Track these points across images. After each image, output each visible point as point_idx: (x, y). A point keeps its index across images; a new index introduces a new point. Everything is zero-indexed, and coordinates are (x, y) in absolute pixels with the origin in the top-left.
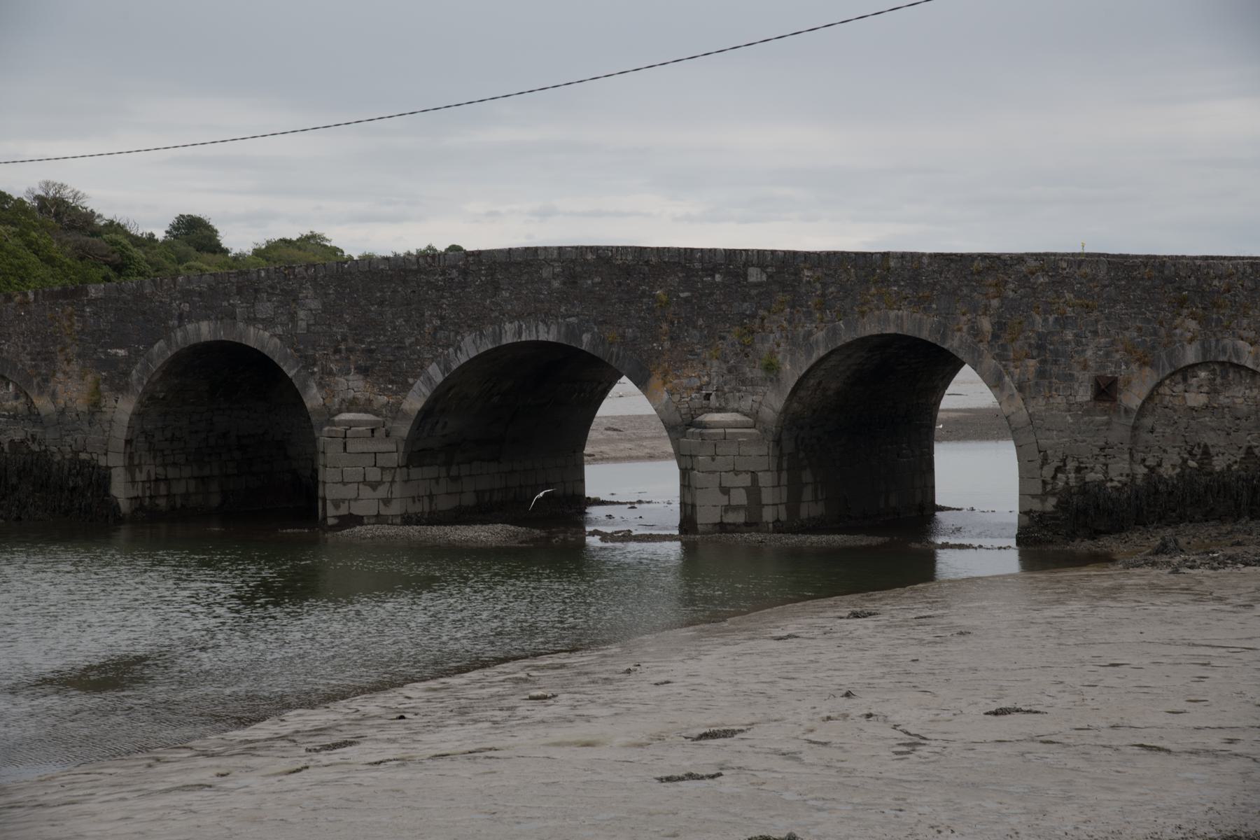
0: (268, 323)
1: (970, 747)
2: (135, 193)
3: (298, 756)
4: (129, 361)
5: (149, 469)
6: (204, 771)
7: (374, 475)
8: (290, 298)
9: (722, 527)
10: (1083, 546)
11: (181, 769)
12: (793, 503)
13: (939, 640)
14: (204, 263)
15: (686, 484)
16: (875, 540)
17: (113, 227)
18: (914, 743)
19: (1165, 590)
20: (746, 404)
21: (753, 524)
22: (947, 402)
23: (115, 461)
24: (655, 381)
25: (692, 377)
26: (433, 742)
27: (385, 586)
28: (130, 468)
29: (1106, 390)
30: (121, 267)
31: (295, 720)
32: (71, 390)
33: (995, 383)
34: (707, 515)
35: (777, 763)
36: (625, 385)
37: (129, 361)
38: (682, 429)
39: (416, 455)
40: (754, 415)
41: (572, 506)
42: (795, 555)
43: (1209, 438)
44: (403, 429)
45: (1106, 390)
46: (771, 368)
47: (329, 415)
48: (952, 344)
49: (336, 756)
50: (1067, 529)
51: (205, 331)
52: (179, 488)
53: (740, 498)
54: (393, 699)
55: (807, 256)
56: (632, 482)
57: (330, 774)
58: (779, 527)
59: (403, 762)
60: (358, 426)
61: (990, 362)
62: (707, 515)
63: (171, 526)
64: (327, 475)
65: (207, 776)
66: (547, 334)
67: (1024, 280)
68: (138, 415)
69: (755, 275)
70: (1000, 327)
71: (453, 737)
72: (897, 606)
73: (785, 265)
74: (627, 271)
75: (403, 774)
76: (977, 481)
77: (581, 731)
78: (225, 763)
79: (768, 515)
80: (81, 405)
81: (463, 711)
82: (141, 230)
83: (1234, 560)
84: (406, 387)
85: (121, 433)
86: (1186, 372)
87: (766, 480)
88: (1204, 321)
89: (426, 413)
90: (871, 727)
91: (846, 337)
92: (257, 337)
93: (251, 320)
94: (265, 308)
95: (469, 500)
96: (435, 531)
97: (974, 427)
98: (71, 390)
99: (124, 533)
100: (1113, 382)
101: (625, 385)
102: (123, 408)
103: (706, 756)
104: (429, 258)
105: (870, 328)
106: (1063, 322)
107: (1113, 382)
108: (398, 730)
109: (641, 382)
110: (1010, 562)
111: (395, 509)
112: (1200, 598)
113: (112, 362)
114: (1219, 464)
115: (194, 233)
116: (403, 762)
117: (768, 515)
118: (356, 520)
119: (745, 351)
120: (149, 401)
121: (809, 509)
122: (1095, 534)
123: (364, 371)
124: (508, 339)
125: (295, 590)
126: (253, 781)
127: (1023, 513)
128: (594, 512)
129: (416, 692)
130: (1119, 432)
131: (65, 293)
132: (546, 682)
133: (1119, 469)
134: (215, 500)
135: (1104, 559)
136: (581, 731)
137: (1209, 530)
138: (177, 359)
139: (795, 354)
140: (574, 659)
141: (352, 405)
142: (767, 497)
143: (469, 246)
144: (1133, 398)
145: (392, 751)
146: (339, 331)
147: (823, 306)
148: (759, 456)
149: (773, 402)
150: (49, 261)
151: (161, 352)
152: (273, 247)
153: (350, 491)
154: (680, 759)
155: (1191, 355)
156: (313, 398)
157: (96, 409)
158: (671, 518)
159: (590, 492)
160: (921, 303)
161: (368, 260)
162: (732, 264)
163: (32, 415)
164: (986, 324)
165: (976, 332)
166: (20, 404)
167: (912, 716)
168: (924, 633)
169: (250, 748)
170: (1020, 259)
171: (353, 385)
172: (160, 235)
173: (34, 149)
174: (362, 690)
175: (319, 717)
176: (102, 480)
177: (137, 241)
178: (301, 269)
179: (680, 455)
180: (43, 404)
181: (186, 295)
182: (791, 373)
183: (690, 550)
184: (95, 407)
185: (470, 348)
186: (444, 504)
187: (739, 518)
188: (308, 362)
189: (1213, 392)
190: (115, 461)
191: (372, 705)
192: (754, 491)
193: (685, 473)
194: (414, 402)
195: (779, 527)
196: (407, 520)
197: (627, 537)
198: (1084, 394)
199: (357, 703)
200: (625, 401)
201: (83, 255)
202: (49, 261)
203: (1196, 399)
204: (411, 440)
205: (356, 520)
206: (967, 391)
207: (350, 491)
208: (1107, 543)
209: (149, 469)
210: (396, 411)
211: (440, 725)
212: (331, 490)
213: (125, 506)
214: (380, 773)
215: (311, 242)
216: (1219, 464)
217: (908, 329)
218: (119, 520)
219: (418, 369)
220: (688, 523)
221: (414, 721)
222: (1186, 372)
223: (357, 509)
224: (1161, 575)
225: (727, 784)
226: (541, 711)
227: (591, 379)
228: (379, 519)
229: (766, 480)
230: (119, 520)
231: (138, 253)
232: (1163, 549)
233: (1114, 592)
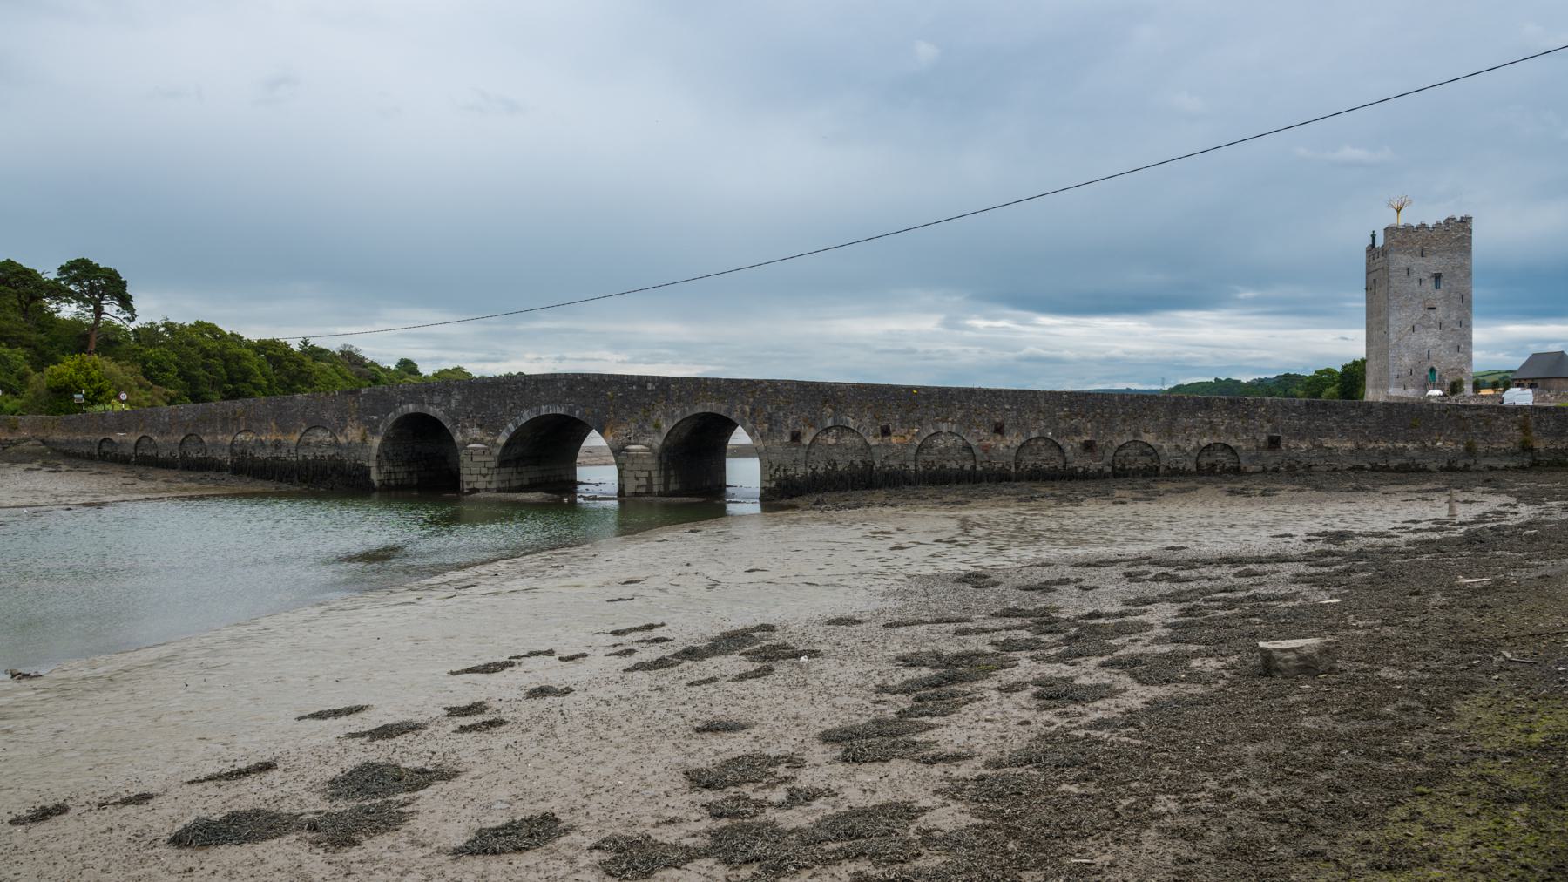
0: (438, 405)
1: (738, 585)
2: (382, 350)
3: (451, 591)
4: (378, 421)
5: (387, 468)
6: (411, 597)
7: (484, 471)
8: (448, 394)
9: (636, 494)
10: (786, 502)
11: (401, 596)
12: (666, 484)
13: (727, 541)
14: (411, 379)
15: (620, 476)
16: (696, 500)
17: (373, 364)
18: (715, 584)
19: (818, 519)
20: (647, 441)
21: (649, 493)
22: (731, 442)
23: (373, 464)
24: (607, 431)
25: (623, 430)
26: (509, 586)
27: (492, 519)
28: (379, 467)
29: (796, 437)
30: (376, 381)
31: (450, 576)
32: (353, 434)
33: (751, 434)
34: (629, 489)
35: (657, 593)
36: (594, 433)
37: (378, 421)
38: (619, 451)
39: (503, 463)
40: (650, 446)
41: (571, 485)
42: (667, 506)
43: (836, 457)
44: (497, 451)
45: (796, 437)
46: (657, 427)
47: (465, 445)
48: (734, 417)
49: (468, 591)
50: (782, 495)
51: (411, 408)
52: (400, 476)
53: (643, 482)
54: (493, 567)
55: (673, 379)
56: (597, 474)
57: (465, 599)
58: (660, 494)
59: (496, 594)
60: (478, 450)
61: (749, 425)
62: (629, 489)
63: (395, 493)
64: (464, 471)
65: (412, 599)
66: (561, 411)
67: (763, 391)
68: (382, 445)
69: (650, 387)
70: (753, 410)
71: (519, 583)
72: (709, 528)
73: (663, 383)
74: (595, 384)
75: (496, 599)
76: (744, 475)
77: (574, 581)
78: (420, 594)
79: (656, 489)
80: (358, 440)
81: (523, 572)
82: (385, 365)
83: (845, 507)
84: (498, 433)
85: (375, 452)
86: (827, 430)
87: (654, 474)
88: (834, 409)
89: (507, 444)
90: (697, 578)
91: (689, 414)
92: (433, 411)
93: (431, 404)
94: (437, 399)
95: (526, 482)
96: (511, 496)
97: (743, 452)
98: (353, 434)
99: (376, 495)
100: (1278, 438)
101: (594, 433)
102: (376, 441)
103: (627, 591)
104: (509, 377)
105: (699, 410)
106: (779, 408)
107: (1278, 438)
108: (495, 580)
109: (601, 432)
110: (756, 508)
111: (494, 486)
112: (831, 523)
113: (372, 421)
114: (840, 468)
115: (407, 366)
116: (496, 594)
117: (656, 489)
118: (477, 490)
119: (646, 419)
120: (387, 438)
121: (673, 486)
122: (791, 497)
123: (480, 426)
124: (543, 413)
125: (452, 520)
126: (432, 601)
127: (763, 488)
128: (581, 488)
129: (502, 564)
130: (801, 455)
131: (351, 392)
132: (559, 560)
133: (801, 470)
134: (415, 482)
135: (794, 507)
136: (574, 581)
137: (836, 495)
138: (398, 421)
139: (666, 422)
140: (571, 550)
141: (475, 441)
142: (655, 481)
143: (527, 373)
144: (806, 441)
145: (492, 589)
146: (469, 408)
147: (679, 400)
148: (652, 464)
149: (658, 441)
150: (346, 378)
151: (392, 417)
152: (441, 372)
153: (474, 478)
154: (616, 592)
155: (829, 423)
156: (458, 438)
157: (363, 442)
158: (614, 489)
159: (579, 479)
160: (721, 400)
161: (482, 378)
162: (641, 381)
163: (337, 444)
164: (747, 409)
165: (743, 412)
166: (332, 440)
167: (715, 574)
168: (719, 538)
169: (431, 587)
170: (761, 382)
171: (475, 432)
172: (393, 367)
173: (341, 330)
174: (483, 563)
175: (461, 574)
176: (367, 472)
177: (383, 370)
178: (453, 383)
179: (617, 463)
180: (342, 439)
181: (403, 393)
182: (666, 428)
183: (622, 503)
184: (364, 440)
185: (527, 416)
186: (515, 484)
187: (643, 490)
188: (456, 422)
189: (838, 438)
190: (373, 464)
191: (484, 570)
192: (649, 479)
193: (620, 471)
194: (502, 440)
195: (660, 494)
196: (499, 490)
197: (595, 498)
198: (787, 439)
199: (477, 568)
200: (595, 440)
201: (359, 375)
202: (346, 378)
203: (831, 441)
204: (500, 456)
205: (477, 490)
206: (740, 437)
207: (474, 478)
208: (796, 501)
209: (387, 468)
210: (494, 443)
211: (513, 578)
212: (465, 478)
213: (377, 484)
214: (486, 598)
215: (458, 370)
216: (840, 468)
217: (715, 411)
218: (374, 490)
219: (504, 425)
220: (621, 493)
221: (502, 577)
222: (827, 430)
223: (477, 486)
224: (817, 513)
225: (636, 603)
226: (557, 573)
227: (730, 426)
228: (487, 490)
229: (654, 474)
230: (374, 490)
231: (383, 375)
232: (817, 503)
233: (798, 521)
